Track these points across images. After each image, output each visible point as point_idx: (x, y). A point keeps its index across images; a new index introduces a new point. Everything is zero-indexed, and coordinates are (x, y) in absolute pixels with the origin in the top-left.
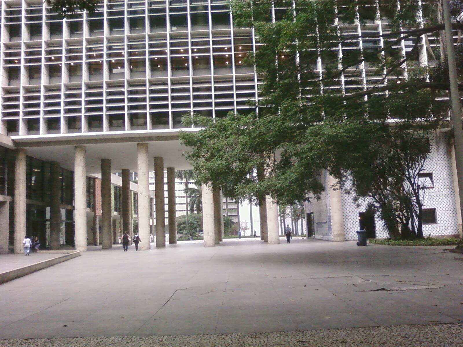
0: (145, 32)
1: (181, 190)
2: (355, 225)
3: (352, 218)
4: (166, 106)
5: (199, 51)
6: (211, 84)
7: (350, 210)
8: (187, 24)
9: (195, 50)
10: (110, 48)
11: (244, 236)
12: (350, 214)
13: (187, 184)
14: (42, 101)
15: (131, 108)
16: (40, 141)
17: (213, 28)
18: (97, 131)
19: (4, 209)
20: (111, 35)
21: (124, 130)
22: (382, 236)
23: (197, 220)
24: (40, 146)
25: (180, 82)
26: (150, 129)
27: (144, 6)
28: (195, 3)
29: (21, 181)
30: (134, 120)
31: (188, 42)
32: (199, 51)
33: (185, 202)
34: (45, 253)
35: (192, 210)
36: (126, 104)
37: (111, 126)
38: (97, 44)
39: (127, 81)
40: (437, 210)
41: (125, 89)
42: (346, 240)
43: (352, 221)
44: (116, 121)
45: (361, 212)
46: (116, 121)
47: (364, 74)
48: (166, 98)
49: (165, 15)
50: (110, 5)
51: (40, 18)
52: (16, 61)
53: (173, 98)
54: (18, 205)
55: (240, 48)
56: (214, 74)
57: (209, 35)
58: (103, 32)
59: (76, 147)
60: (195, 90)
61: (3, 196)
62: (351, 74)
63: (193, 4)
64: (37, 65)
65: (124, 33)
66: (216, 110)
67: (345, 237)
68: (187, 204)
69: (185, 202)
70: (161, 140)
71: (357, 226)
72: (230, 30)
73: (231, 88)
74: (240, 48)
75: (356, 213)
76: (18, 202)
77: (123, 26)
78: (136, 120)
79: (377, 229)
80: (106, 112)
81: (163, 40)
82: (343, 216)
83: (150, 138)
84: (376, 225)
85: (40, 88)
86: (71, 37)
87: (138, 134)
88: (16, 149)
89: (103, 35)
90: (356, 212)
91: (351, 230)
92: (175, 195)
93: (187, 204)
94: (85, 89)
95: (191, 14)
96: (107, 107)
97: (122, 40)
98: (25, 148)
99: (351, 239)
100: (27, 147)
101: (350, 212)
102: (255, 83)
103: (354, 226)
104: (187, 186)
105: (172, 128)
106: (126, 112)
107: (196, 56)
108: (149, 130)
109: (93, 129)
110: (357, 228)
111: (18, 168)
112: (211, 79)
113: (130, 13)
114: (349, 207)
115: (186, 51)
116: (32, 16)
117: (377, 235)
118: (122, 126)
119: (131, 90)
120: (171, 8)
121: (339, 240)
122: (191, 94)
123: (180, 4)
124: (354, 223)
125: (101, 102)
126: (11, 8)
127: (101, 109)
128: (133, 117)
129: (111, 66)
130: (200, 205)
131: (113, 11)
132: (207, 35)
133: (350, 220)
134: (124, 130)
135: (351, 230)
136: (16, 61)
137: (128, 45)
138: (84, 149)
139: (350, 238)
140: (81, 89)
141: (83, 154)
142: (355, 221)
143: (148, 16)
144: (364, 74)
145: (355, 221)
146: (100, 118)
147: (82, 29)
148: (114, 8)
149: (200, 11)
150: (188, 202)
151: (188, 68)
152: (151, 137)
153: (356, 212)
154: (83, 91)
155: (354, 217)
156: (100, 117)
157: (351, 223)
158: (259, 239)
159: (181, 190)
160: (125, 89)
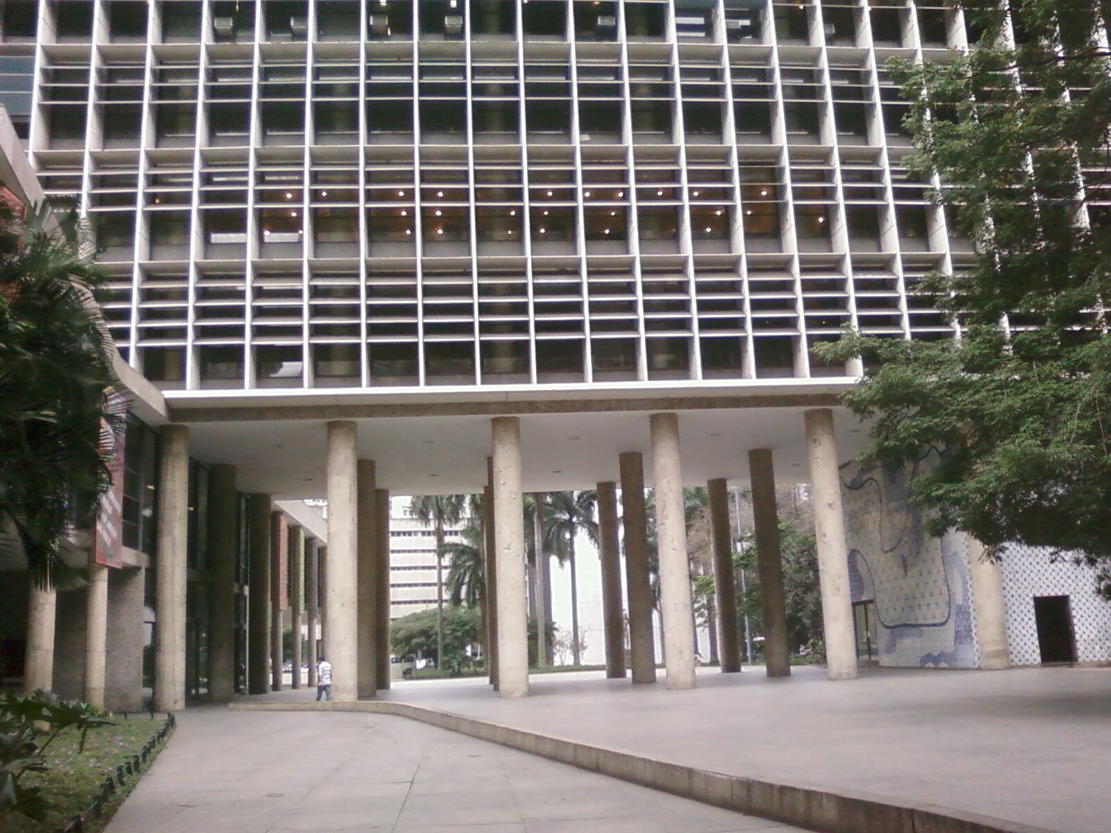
0: (139, 147)
1: (429, 551)
2: (1027, 627)
3: (1018, 611)
4: (412, 329)
5: (332, 197)
6: (527, 278)
7: (1013, 592)
8: (411, 128)
9: (401, 194)
10: (207, 179)
11: (563, 666)
12: (1013, 600)
13: (440, 534)
14: (135, 305)
15: (316, 331)
16: (287, 404)
17: (422, 142)
18: (394, 385)
19: (132, 589)
20: (51, 148)
21: (242, 387)
22: (1091, 656)
23: (454, 626)
24: (235, 419)
25: (757, 267)
26: (309, 387)
27: (357, 78)
28: (377, 78)
29: (178, 512)
30: (210, 365)
31: (412, 172)
32: (332, 197)
33: (436, 580)
34: (254, 710)
35: (456, 600)
36: (305, 321)
37: (205, 377)
38: (388, 164)
39: (197, 265)
40: (1072, 597)
41: (247, 285)
42: (1011, 668)
43: (1019, 620)
44: (221, 363)
45: (1038, 595)
46: (776, 355)
47: (848, 266)
48: (577, 308)
49: (303, 104)
50: (162, 71)
51: (83, 94)
52: (289, 196)
53: (429, 310)
54: (168, 578)
55: (764, 193)
56: (424, 254)
57: (357, 158)
58: (248, 137)
59: (331, 426)
60: (484, 291)
61: (135, 551)
62: (462, 270)
63: (373, 78)
64: (277, 209)
65: (248, 143)
66: (426, 344)
67: (1012, 657)
68: (440, 584)
69: (436, 580)
70: (560, 411)
71: (1031, 631)
72: (413, 148)
73: (467, 291)
74: (550, 194)
75: (1028, 599)
76: (169, 570)
77: (245, 126)
78: (723, 357)
79: (1077, 637)
80: (137, 342)
81: (239, 166)
82: (1006, 605)
83: (531, 405)
84: (1076, 628)
85: (129, 270)
86: (104, 147)
87: (336, 396)
88: (169, 426)
89: (194, 145)
90: (1027, 596)
91: (1018, 640)
92: (389, 564)
93: (440, 584)
94: (140, 280)
95: (368, 104)
96: (196, 328)
97: (187, 160)
98: (187, 424)
99: (1020, 664)
100: (358, 416)
101: (1012, 596)
102: (472, 280)
103: (1024, 632)
104: (440, 540)
105: (367, 386)
106: (247, 341)
107: (401, 209)
108: (697, 381)
109: (382, 379)
110: (1032, 635)
111: (169, 477)
112: (415, 267)
113: (318, 90)
114: (1011, 584)
115: (410, 195)
116: (55, 87)
117: (1079, 653)
118: (237, 379)
119: (150, 290)
120: (265, 86)
121: (998, 666)
122: (476, 300)
123: (344, 78)
124: (1023, 623)
125: (631, 307)
126: (161, 64)
127: (238, 331)
128: (207, 357)
129: (213, 222)
130: (652, 577)
131: (167, 87)
132: (462, 157)
133: (1015, 616)
134: (242, 387)
135: (1018, 640)
136: (289, 196)
137: (256, 173)
138: (352, 427)
139: (1016, 660)
140: (186, 279)
141: (352, 444)
142: (1026, 619)
143: (259, 104)
144: (848, 266)
145: (1026, 619)
146: (736, 346)
147: (192, 127)
148: (170, 81)
149: (185, 99)
150: (444, 580)
151: (412, 238)
152: (536, 402)
153: (1027, 596)
154: (136, 286)
155: (1022, 607)
156: (738, 344)
157: (1016, 624)
158: (603, 675)
159: (429, 551)
160: (305, 284)
